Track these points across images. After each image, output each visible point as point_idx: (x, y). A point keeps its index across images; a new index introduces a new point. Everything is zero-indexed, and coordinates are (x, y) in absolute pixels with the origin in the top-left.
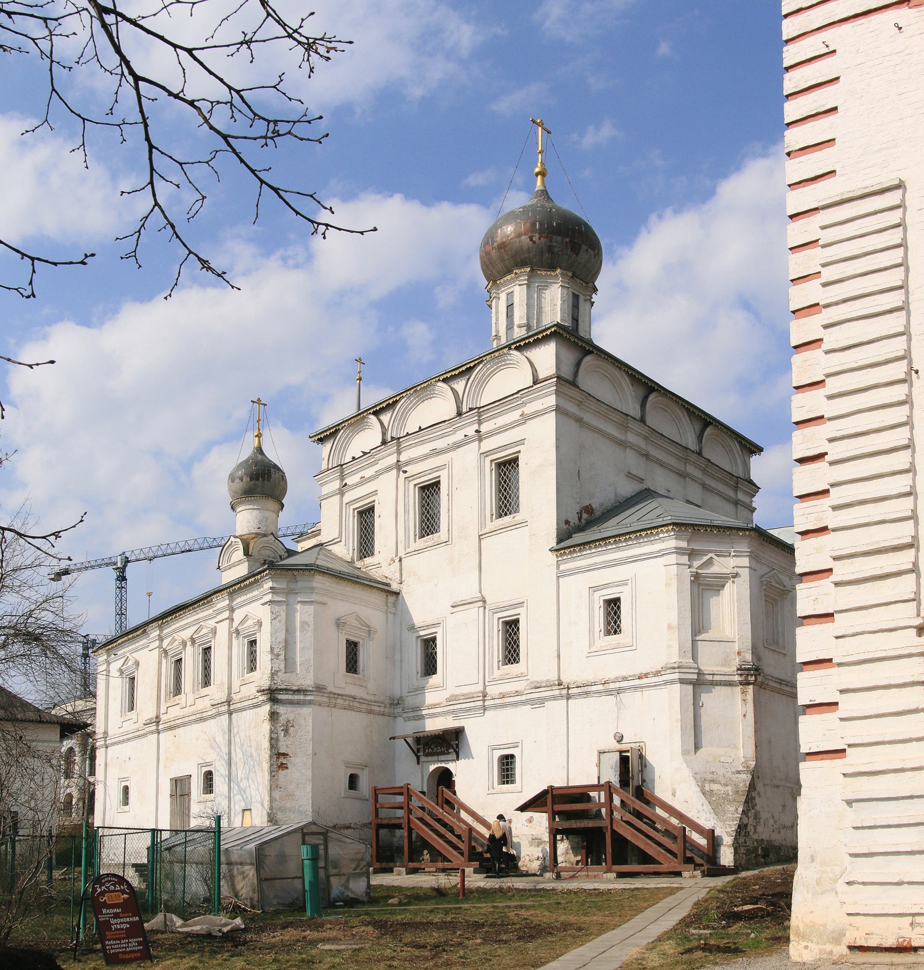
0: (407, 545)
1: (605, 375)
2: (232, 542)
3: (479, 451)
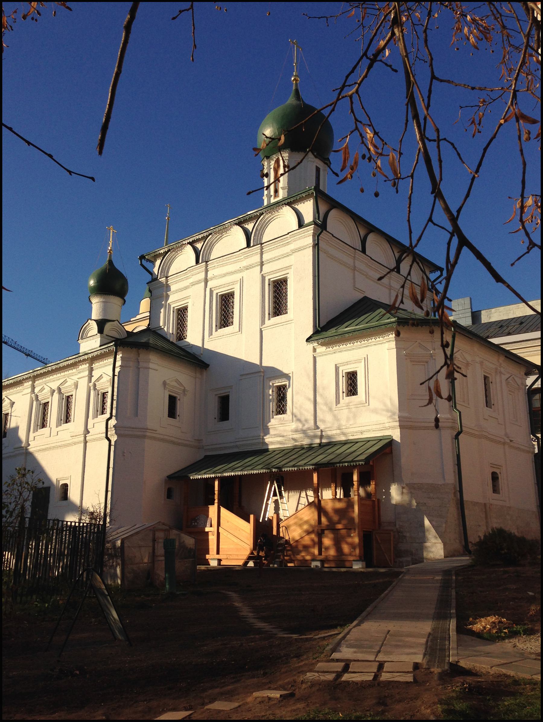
0: (211, 334)
1: (340, 222)
2: (89, 324)
3: (261, 273)
